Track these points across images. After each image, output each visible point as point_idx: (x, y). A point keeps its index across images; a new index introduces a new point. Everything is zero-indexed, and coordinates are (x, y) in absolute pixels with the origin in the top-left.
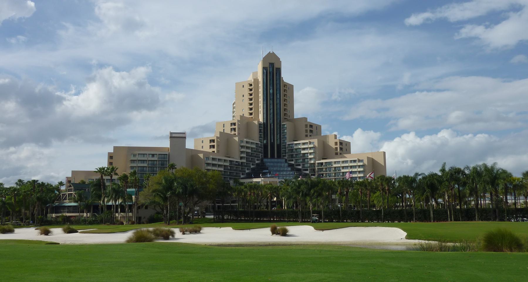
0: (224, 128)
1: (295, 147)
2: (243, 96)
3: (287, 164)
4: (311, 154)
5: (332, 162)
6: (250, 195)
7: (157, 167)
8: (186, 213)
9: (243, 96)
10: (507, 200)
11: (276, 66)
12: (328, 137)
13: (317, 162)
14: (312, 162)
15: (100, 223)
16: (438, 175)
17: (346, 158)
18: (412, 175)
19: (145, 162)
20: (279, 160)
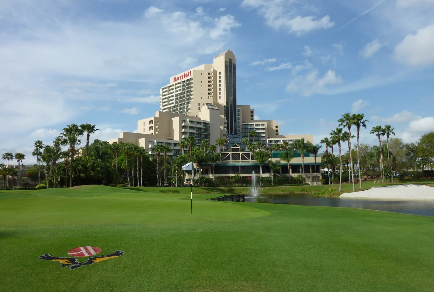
0: (199, 107)
1: (250, 127)
2: (201, 82)
3: (380, 135)
4: (263, 133)
5: (273, 140)
6: (158, 160)
7: (248, 133)
8: (155, 174)
9: (201, 82)
10: (428, 171)
11: (233, 62)
12: (272, 121)
13: (268, 139)
14: (264, 139)
15: (277, 184)
16: (75, 155)
17: (286, 138)
18: (10, 153)
19: (253, 125)
20: (235, 136)
